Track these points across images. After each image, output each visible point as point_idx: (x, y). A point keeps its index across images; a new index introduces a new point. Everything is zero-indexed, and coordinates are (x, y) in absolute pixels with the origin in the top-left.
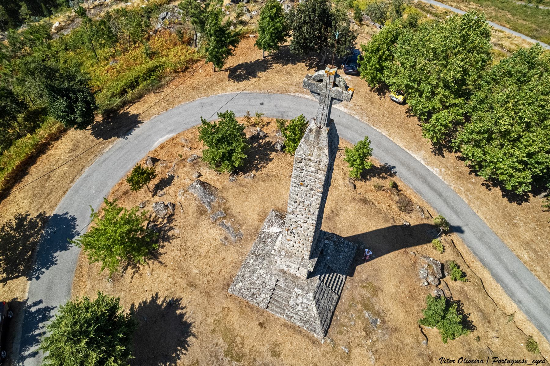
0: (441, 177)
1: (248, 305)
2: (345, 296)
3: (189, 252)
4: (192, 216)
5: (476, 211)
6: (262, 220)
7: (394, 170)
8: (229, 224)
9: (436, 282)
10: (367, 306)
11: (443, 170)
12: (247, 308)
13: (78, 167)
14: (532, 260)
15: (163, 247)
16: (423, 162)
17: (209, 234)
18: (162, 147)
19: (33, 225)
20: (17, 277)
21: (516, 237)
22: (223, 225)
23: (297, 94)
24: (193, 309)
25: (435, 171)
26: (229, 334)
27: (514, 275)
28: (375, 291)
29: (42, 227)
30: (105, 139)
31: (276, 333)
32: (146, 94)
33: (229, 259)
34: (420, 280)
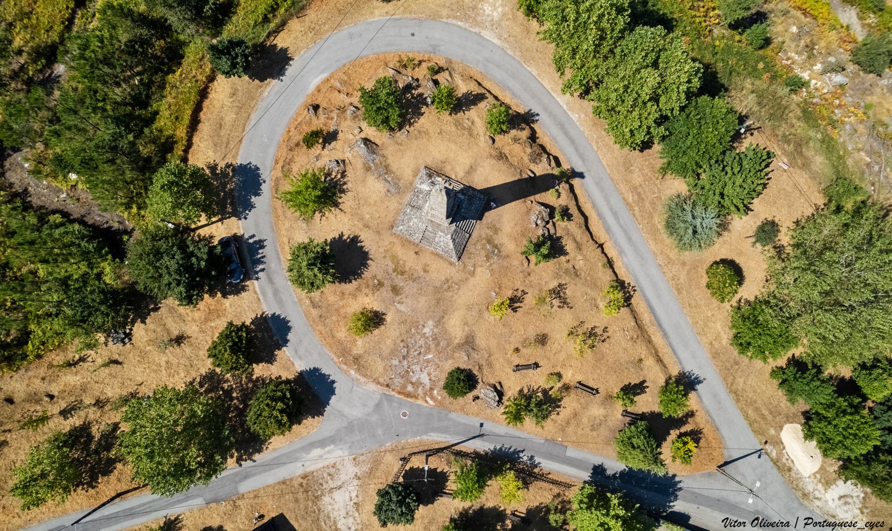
0: (578, 124)
1: (407, 240)
2: (474, 235)
3: (362, 202)
4: (360, 172)
5: (601, 157)
6: (415, 175)
7: (537, 118)
8: (390, 179)
9: (544, 223)
10: (489, 241)
11: (582, 116)
12: (406, 242)
13: (245, 115)
14: (634, 202)
15: (340, 198)
16: (565, 107)
17: (374, 187)
18: (319, 90)
19: (224, 174)
20: (229, 217)
21: (628, 182)
22: (386, 180)
23: (449, 21)
24: (368, 242)
25: (574, 117)
26: (394, 258)
27: (615, 214)
28: (496, 230)
29: (233, 176)
30: (262, 80)
31: (426, 258)
32: (290, 19)
33: (392, 208)
34: (530, 223)
